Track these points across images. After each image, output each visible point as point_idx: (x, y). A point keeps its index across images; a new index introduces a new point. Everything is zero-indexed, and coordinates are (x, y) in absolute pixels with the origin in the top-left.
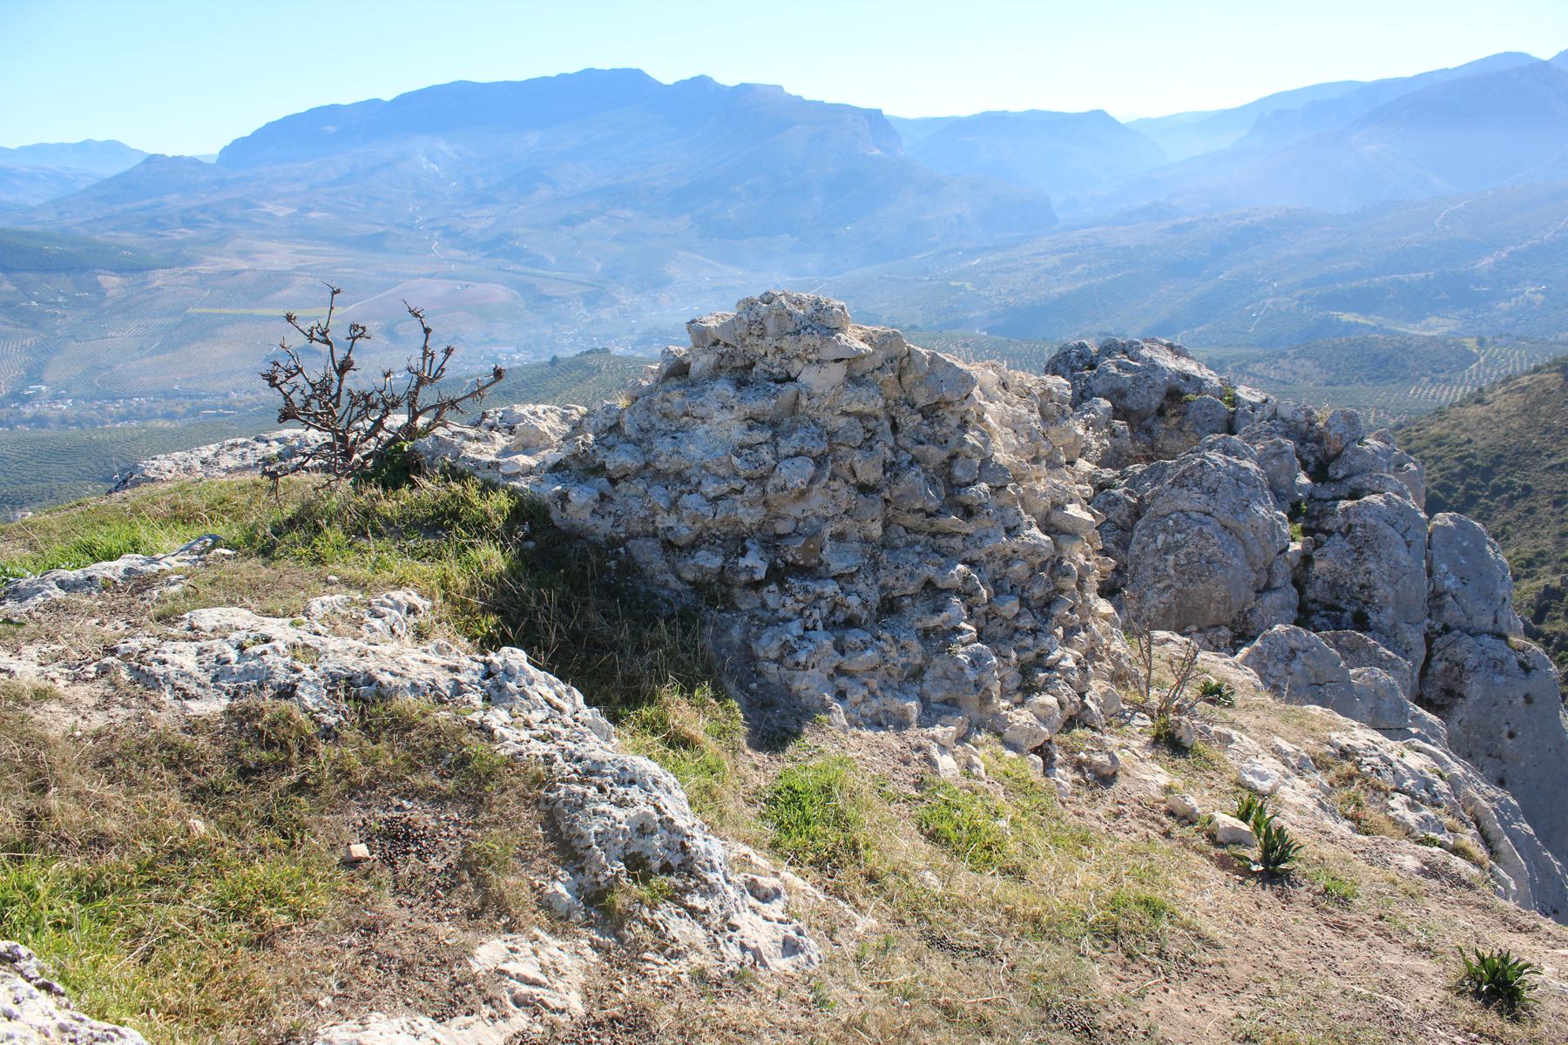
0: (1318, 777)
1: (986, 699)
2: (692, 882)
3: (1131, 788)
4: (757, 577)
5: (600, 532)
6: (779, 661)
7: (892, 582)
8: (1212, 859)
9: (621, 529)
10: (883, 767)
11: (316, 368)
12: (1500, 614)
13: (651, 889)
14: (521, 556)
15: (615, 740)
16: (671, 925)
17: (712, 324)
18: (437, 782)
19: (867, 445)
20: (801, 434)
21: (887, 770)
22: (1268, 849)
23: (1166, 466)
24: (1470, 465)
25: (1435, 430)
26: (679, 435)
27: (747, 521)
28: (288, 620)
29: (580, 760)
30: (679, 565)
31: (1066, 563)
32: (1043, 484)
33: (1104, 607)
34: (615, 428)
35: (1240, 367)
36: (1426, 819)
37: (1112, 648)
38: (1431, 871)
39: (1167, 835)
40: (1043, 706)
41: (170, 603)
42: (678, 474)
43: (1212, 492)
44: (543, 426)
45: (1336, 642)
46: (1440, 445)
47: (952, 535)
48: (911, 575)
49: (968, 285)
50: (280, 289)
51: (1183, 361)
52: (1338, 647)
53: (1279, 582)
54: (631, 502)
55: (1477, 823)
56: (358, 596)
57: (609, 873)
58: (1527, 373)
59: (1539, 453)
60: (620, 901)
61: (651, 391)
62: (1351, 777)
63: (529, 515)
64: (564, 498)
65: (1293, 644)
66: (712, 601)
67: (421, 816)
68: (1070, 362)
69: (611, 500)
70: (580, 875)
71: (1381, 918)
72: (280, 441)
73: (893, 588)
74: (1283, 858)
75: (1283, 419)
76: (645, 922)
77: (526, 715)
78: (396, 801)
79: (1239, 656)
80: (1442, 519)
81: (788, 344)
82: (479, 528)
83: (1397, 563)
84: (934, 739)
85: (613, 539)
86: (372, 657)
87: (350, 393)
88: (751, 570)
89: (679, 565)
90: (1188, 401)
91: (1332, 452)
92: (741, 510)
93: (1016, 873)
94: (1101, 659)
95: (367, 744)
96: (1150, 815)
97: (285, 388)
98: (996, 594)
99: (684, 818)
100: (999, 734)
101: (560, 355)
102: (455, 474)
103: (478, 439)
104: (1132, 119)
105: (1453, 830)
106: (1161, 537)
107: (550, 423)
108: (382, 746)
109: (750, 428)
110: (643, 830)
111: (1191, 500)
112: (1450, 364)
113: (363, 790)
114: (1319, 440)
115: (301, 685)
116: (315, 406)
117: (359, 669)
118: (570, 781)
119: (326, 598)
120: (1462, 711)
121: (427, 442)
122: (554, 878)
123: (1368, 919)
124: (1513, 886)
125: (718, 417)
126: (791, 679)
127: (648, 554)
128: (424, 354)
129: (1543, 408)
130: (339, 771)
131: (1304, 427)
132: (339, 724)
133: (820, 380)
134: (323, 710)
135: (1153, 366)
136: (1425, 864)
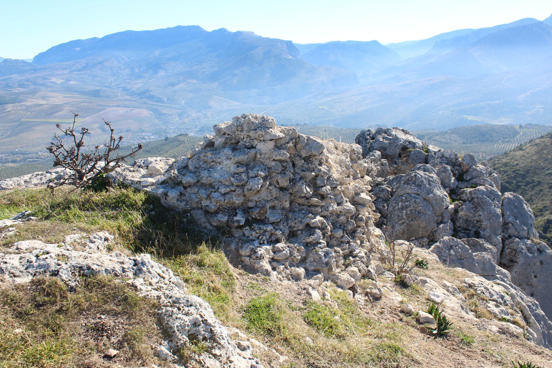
0: (461, 296)
1: (330, 269)
2: (215, 344)
3: (387, 302)
4: (241, 224)
5: (180, 207)
6: (250, 256)
7: (293, 225)
8: (418, 329)
9: (188, 206)
10: (290, 296)
11: (69, 144)
12: (530, 230)
13: (199, 348)
14: (150, 217)
15: (186, 289)
16: (206, 361)
17: (223, 126)
18: (115, 308)
19: (283, 172)
20: (257, 168)
21: (292, 298)
22: (440, 324)
23: (402, 176)
24: (518, 173)
25: (504, 161)
26: (210, 169)
27: (237, 202)
28: (57, 245)
29: (171, 297)
30: (211, 220)
31: (360, 216)
32: (352, 185)
33: (378, 231)
34: (186, 167)
35: (430, 138)
36: (502, 311)
37: (380, 248)
38: (502, 331)
39: (401, 320)
40: (353, 271)
41: (9, 239)
42: (210, 185)
43: (419, 186)
44: (158, 167)
45: (468, 243)
46: (506, 166)
47: (316, 206)
48: (301, 222)
49: (326, 108)
50: (58, 112)
51: (408, 136)
52: (469, 245)
53: (446, 220)
54: (192, 196)
55: (522, 311)
56: (85, 234)
57: (182, 342)
58: (538, 138)
59: (543, 168)
60: (186, 353)
61: (200, 152)
62: (473, 295)
63: (152, 201)
64: (166, 195)
65: (451, 244)
66: (224, 233)
67: (108, 321)
68: (361, 139)
69: (185, 195)
70: (171, 343)
71: (483, 350)
72: (56, 173)
73: (294, 227)
74: (446, 328)
75: (446, 158)
76: (196, 360)
77: (150, 280)
78: (98, 315)
79: (431, 249)
80: (507, 195)
81: (252, 134)
82: (133, 206)
83: (490, 212)
84: (310, 285)
85: (185, 210)
86: (89, 259)
87: (82, 154)
88: (239, 221)
89: (211, 220)
90: (410, 151)
91: (465, 170)
92: (235, 198)
93: (340, 337)
94: (375, 252)
95: (87, 293)
96: (394, 312)
97: (56, 153)
98: (334, 229)
99: (211, 319)
100: (335, 283)
101: (169, 136)
102: (123, 185)
103: (134, 171)
104: (387, 44)
105: (512, 315)
106: (400, 204)
107: (160, 165)
108: (93, 294)
109: (238, 167)
110: (195, 324)
111: (411, 189)
112: (509, 135)
113: (85, 311)
114: (460, 165)
115: (61, 270)
116: (68, 160)
117: (84, 264)
118: (167, 306)
119: (72, 236)
120: (517, 268)
121: (113, 173)
122: (161, 344)
123: (478, 351)
124: (536, 336)
125: (225, 162)
126: (255, 263)
127: (199, 215)
128: (111, 139)
129: (545, 151)
130: (75, 304)
131: (454, 160)
132: (77, 286)
133: (265, 148)
134: (70, 280)
135: (396, 138)
136: (500, 329)
